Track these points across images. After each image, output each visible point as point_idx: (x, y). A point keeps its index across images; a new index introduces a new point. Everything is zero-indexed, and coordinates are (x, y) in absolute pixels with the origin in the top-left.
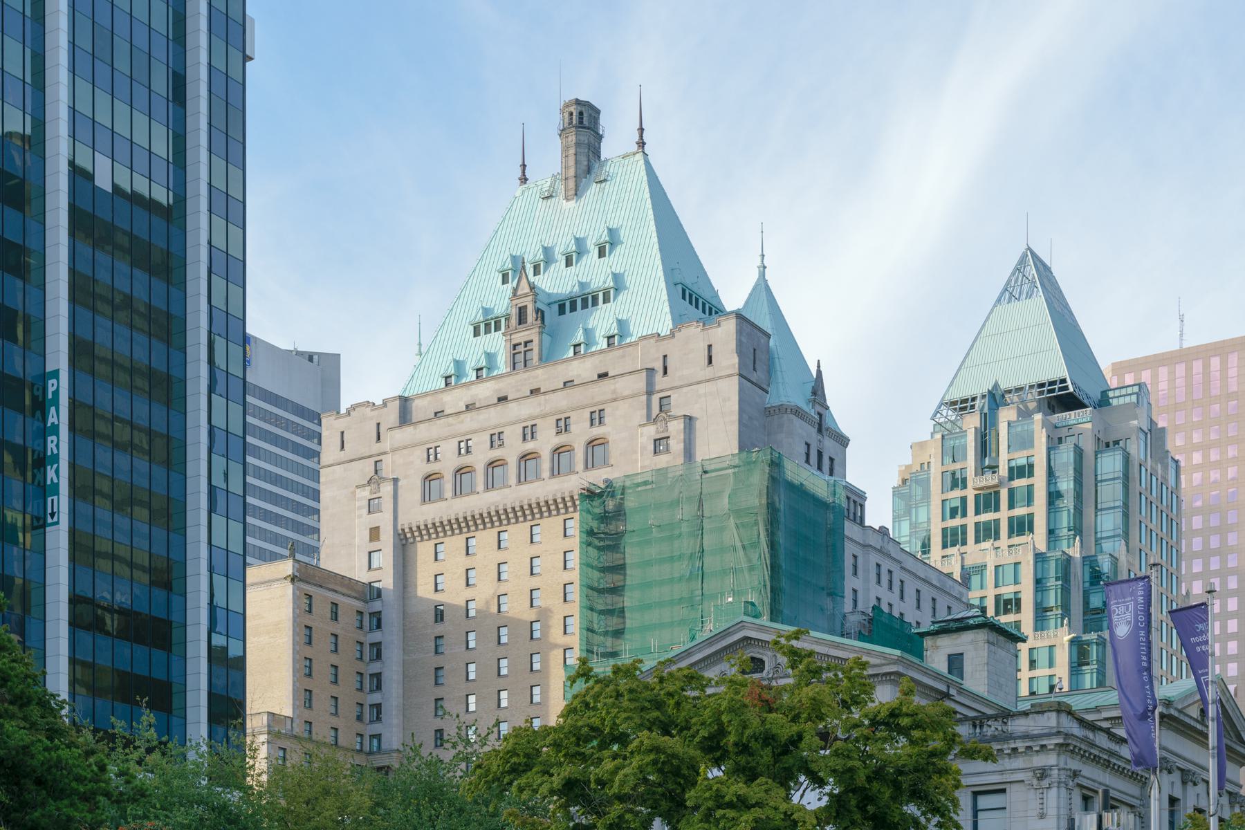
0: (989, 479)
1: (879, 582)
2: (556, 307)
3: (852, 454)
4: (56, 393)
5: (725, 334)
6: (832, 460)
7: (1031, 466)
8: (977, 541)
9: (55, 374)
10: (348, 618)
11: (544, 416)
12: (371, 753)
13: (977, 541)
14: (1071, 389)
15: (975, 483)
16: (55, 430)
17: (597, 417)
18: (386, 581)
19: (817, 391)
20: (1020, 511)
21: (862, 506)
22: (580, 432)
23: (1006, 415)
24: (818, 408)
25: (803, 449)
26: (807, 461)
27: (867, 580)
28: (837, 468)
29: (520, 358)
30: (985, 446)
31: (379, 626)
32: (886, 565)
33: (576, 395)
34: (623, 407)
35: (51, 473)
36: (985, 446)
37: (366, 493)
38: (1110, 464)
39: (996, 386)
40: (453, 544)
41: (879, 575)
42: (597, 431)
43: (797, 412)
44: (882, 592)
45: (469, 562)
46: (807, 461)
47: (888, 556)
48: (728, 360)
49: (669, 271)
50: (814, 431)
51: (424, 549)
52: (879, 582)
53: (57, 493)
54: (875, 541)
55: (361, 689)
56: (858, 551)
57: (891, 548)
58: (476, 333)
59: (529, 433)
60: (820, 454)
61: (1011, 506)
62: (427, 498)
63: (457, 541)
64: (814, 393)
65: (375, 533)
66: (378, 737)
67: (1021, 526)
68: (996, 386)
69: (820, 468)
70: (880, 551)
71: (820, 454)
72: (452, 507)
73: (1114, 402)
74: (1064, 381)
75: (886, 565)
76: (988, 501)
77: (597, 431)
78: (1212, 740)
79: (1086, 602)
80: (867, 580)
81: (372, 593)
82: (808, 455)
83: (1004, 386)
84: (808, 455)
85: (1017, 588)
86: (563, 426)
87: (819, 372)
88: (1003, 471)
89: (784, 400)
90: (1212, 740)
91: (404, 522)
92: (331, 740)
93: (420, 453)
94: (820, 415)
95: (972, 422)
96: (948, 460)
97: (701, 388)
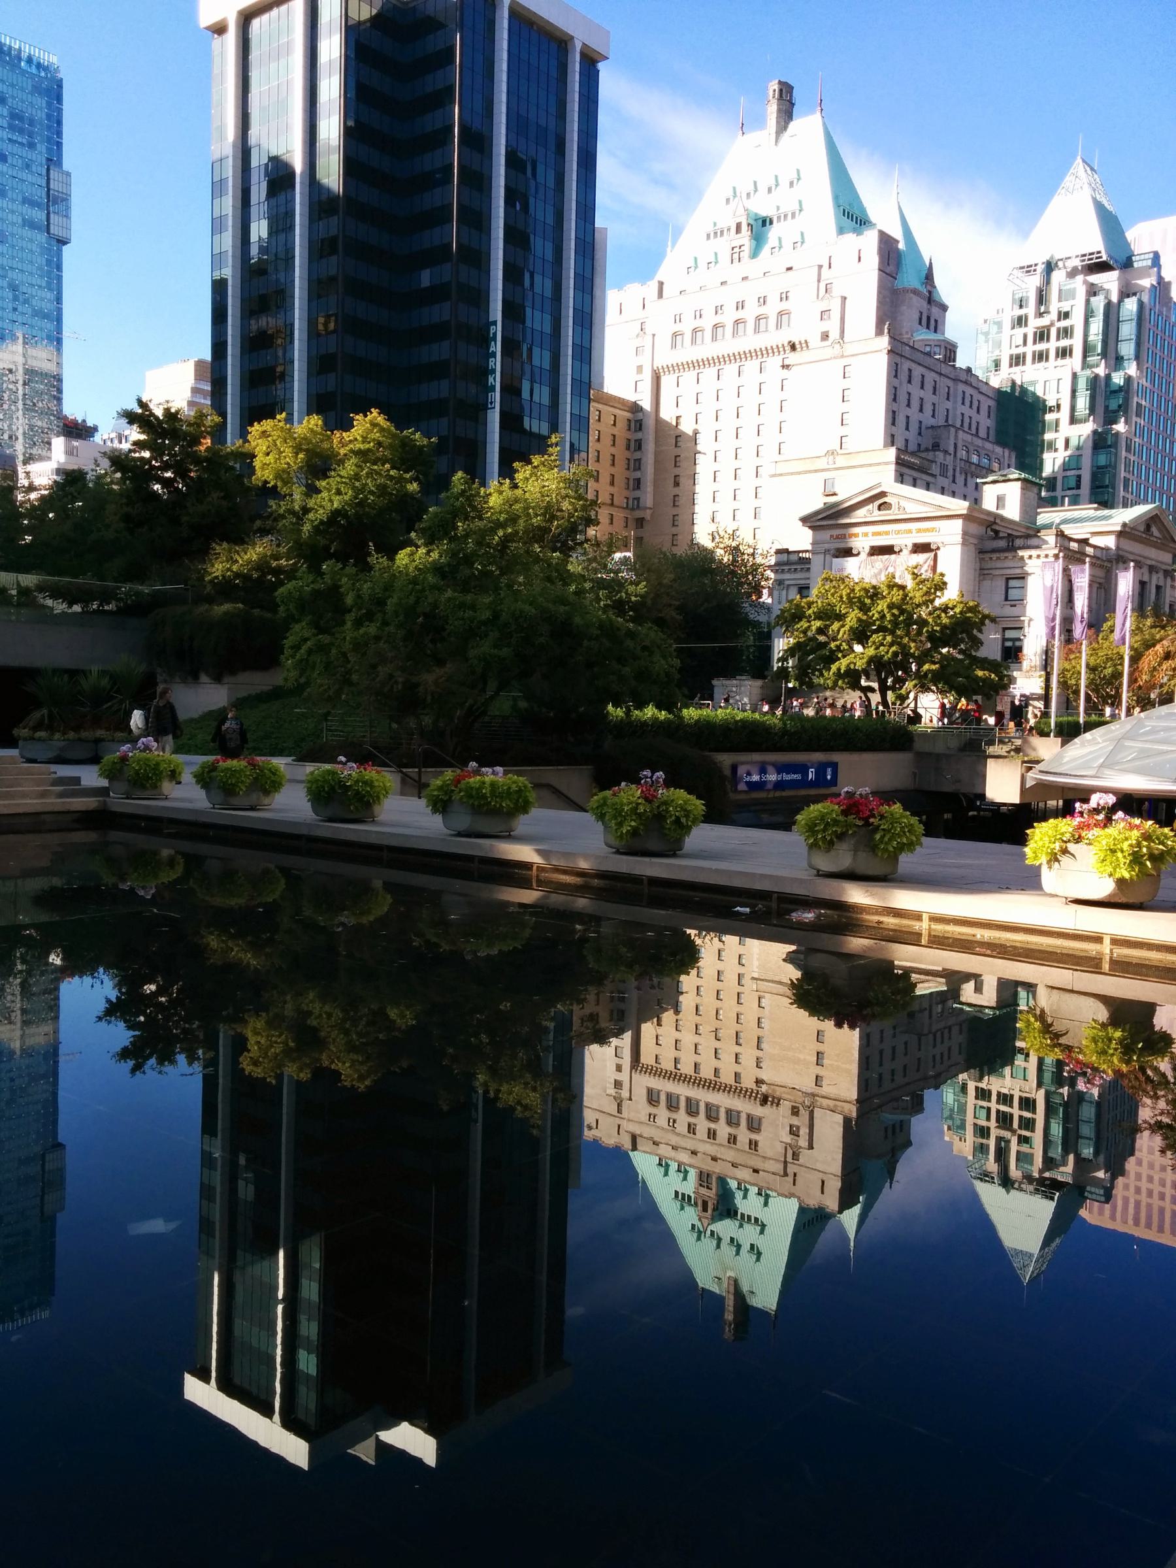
0: (1044, 321)
1: (963, 403)
2: (760, 222)
3: (950, 317)
4: (495, 334)
5: (870, 241)
6: (936, 321)
7: (1059, 406)
8: (1033, 363)
9: (495, 323)
10: (622, 425)
12: (633, 509)
13: (1033, 363)
14: (1104, 258)
15: (1034, 323)
16: (494, 355)
17: (784, 297)
18: (647, 405)
19: (929, 277)
21: (955, 353)
22: (772, 309)
23: (1058, 276)
24: (929, 288)
25: (917, 316)
26: (920, 323)
28: (939, 327)
29: (736, 256)
30: (1042, 298)
31: (640, 429)
35: (491, 380)
36: (1042, 298)
38: (1131, 305)
39: (1052, 257)
40: (689, 376)
41: (963, 399)
43: (915, 292)
44: (966, 410)
46: (920, 323)
48: (872, 260)
49: (836, 198)
50: (925, 304)
51: (667, 381)
52: (963, 403)
53: (494, 391)
54: (963, 377)
55: (628, 469)
56: (950, 383)
57: (972, 380)
58: (708, 236)
59: (740, 305)
60: (929, 318)
62: (674, 346)
63: (692, 374)
64: (927, 278)
65: (640, 369)
66: (638, 499)
67: (1064, 353)
68: (1052, 257)
69: (928, 327)
70: (966, 382)
71: (929, 318)
72: (688, 353)
73: (1136, 265)
74: (1099, 252)
76: (1042, 335)
77: (784, 306)
79: (1107, 407)
80: (955, 402)
81: (635, 408)
82: (920, 319)
83: (1057, 257)
84: (920, 319)
85: (1058, 396)
87: (931, 264)
88: (1054, 315)
89: (906, 285)
91: (658, 363)
92: (609, 502)
94: (930, 292)
95: (1035, 281)
96: (1016, 307)
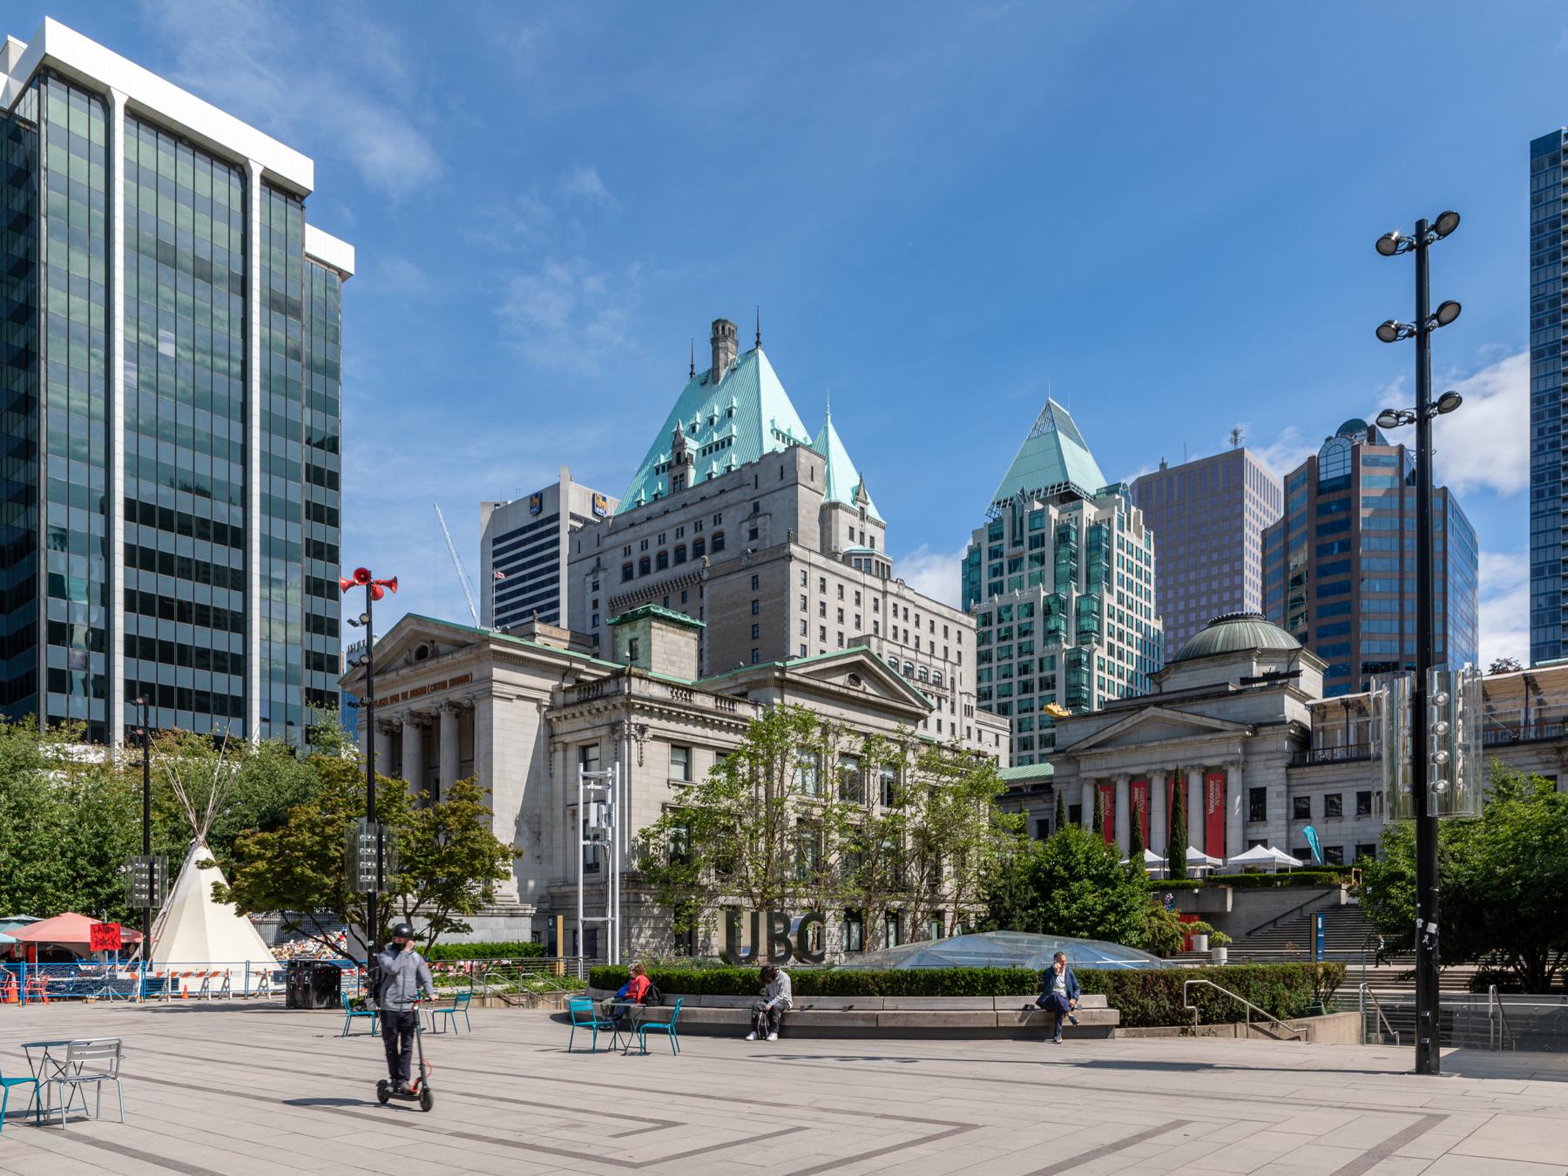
11: (687, 521)
17: (718, 520)
20: (1047, 673)
27: (885, 615)
32: (901, 604)
33: (706, 506)
34: (732, 511)
37: (590, 579)
42: (718, 528)
45: (755, 644)
47: (904, 598)
60: (862, 534)
61: (1041, 670)
70: (896, 595)
71: (862, 534)
75: (901, 604)
78: (564, 621)
80: (885, 615)
86: (698, 527)
90: (564, 621)
93: (620, 551)
97: (777, 495)
